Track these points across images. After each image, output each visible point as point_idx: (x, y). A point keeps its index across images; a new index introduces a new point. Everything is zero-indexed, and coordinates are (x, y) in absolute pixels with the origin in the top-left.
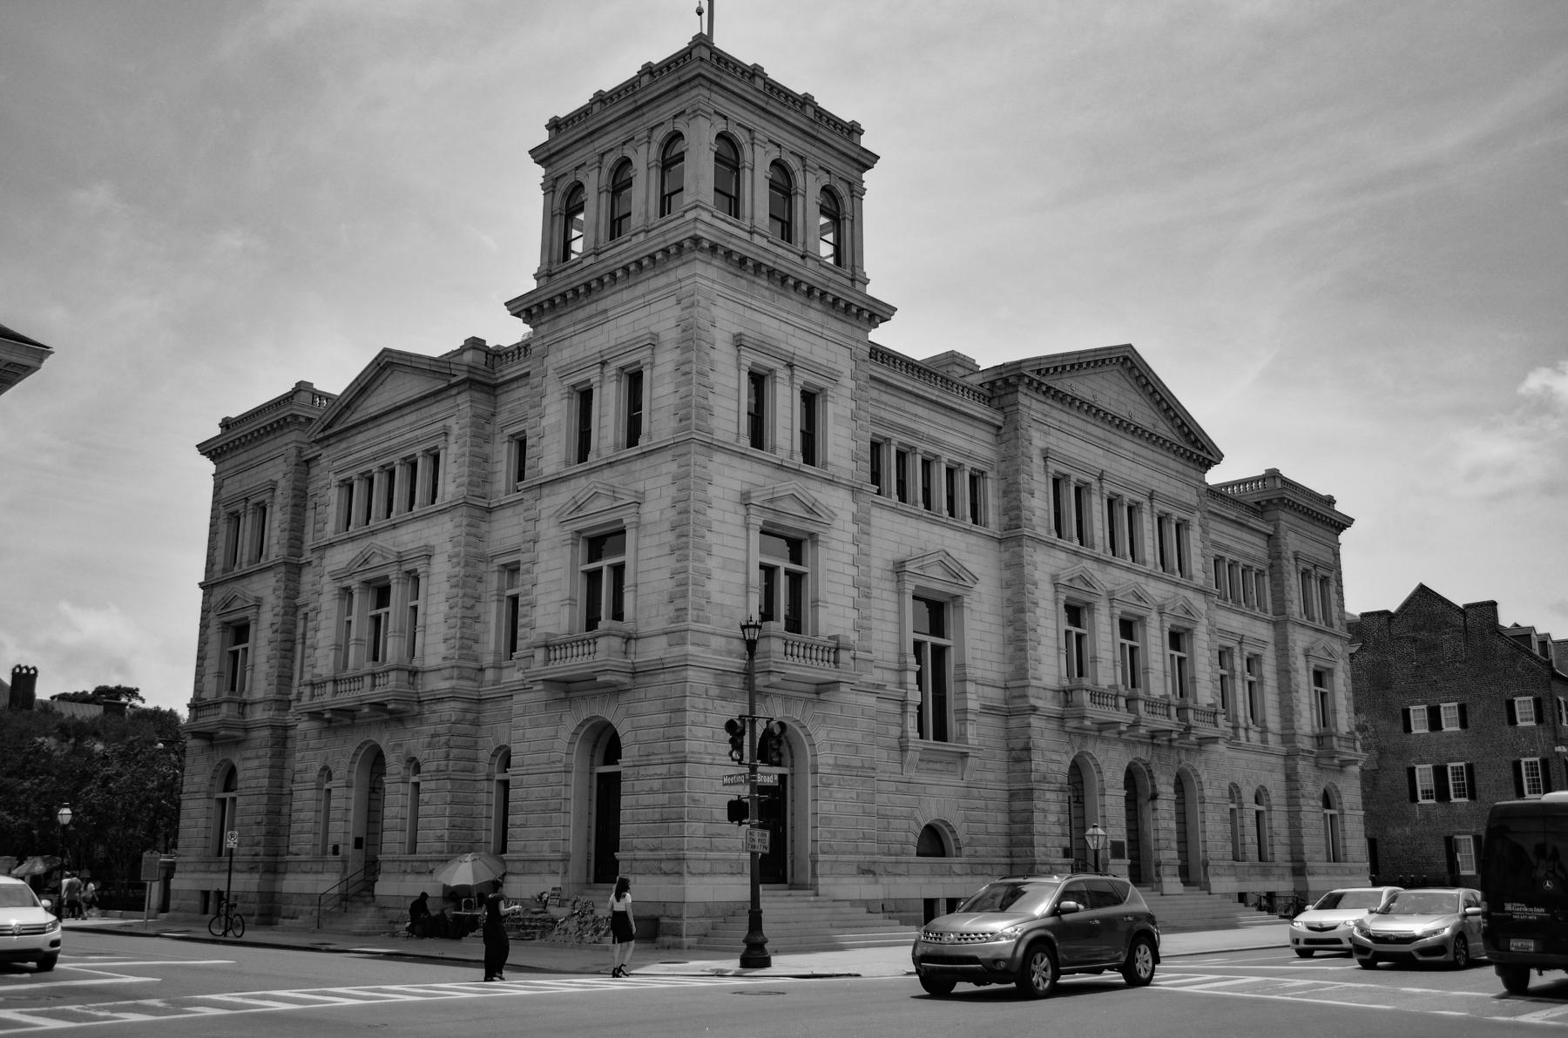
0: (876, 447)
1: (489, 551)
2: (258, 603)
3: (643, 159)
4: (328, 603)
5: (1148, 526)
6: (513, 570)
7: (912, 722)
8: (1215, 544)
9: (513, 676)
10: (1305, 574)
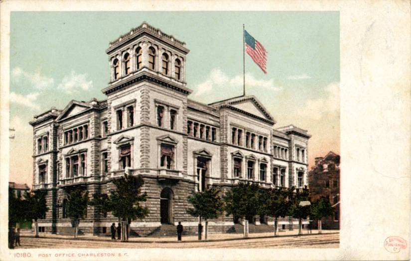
2: (47, 161)
3: (120, 58)
4: (64, 162)
5: (243, 135)
8: (274, 143)
9: (107, 179)
10: (298, 150)
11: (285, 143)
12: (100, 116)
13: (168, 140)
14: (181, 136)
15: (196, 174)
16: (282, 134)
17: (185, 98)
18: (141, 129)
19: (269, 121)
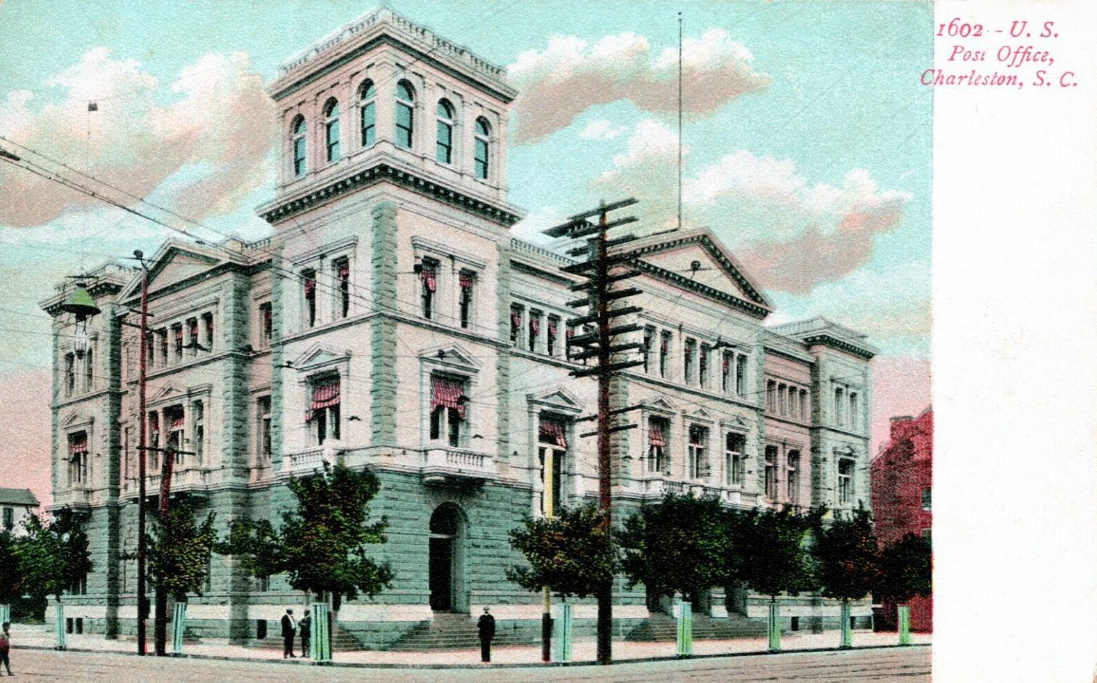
6: (265, 402)
15: (537, 462)
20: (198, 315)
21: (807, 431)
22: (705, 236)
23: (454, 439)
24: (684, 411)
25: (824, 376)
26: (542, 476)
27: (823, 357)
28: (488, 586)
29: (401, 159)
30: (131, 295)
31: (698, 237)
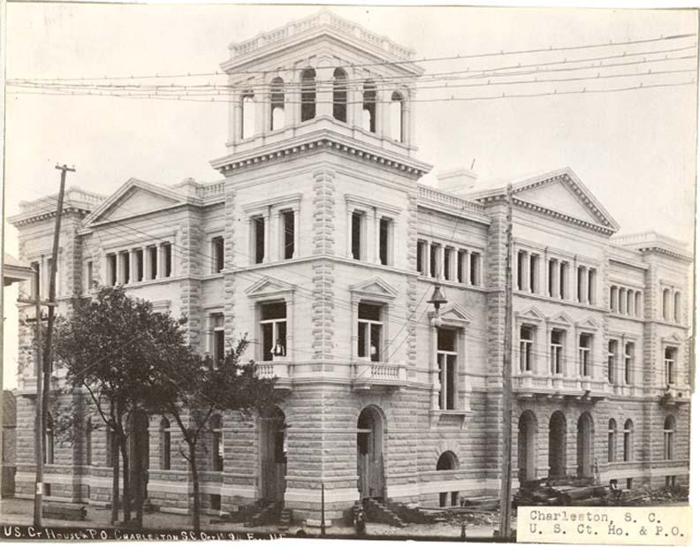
0: (420, 245)
1: (205, 306)
7: (436, 400)
11: (449, 425)
12: (204, 222)
13: (375, 290)
14: (405, 279)
15: (436, 367)
16: (630, 256)
17: (412, 184)
18: (314, 268)
19: (602, 226)
20: (157, 243)
21: (640, 325)
22: (565, 175)
23: (375, 358)
24: (547, 319)
25: (655, 282)
26: (440, 378)
27: (654, 264)
28: (401, 469)
29: (339, 132)
30: (97, 220)
31: (560, 176)
